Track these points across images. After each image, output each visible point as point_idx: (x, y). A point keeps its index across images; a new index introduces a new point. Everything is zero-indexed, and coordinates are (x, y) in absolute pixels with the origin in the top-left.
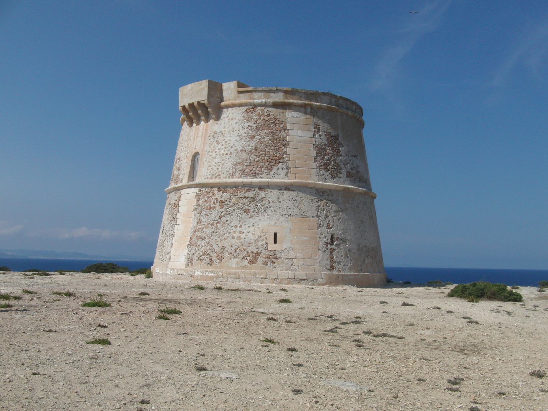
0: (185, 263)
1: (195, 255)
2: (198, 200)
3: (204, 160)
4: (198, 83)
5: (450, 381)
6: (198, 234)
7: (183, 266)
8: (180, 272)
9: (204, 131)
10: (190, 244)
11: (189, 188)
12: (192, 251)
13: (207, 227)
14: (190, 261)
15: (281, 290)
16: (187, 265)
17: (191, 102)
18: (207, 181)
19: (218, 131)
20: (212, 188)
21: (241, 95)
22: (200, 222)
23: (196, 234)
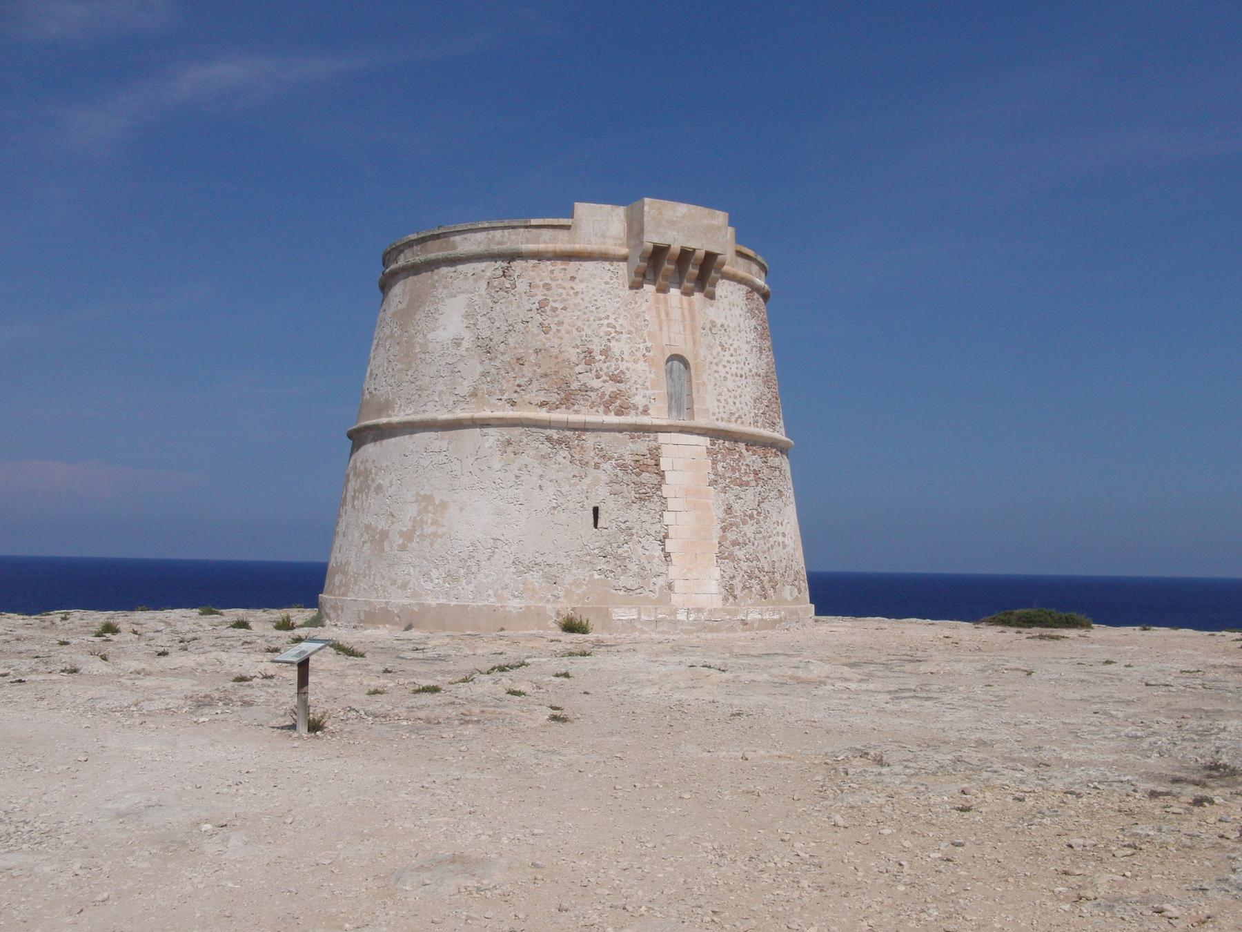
0: (721, 597)
1: (738, 579)
2: (714, 462)
3: (705, 378)
4: (707, 210)
5: (1211, 802)
6: (731, 536)
7: (718, 603)
8: (718, 617)
9: (686, 312)
10: (721, 557)
11: (681, 432)
12: (731, 572)
13: (745, 523)
14: (729, 591)
15: (417, 692)
16: (726, 599)
17: (691, 245)
18: (722, 425)
19: (719, 322)
20: (736, 442)
21: (740, 260)
22: (729, 509)
23: (728, 535)
